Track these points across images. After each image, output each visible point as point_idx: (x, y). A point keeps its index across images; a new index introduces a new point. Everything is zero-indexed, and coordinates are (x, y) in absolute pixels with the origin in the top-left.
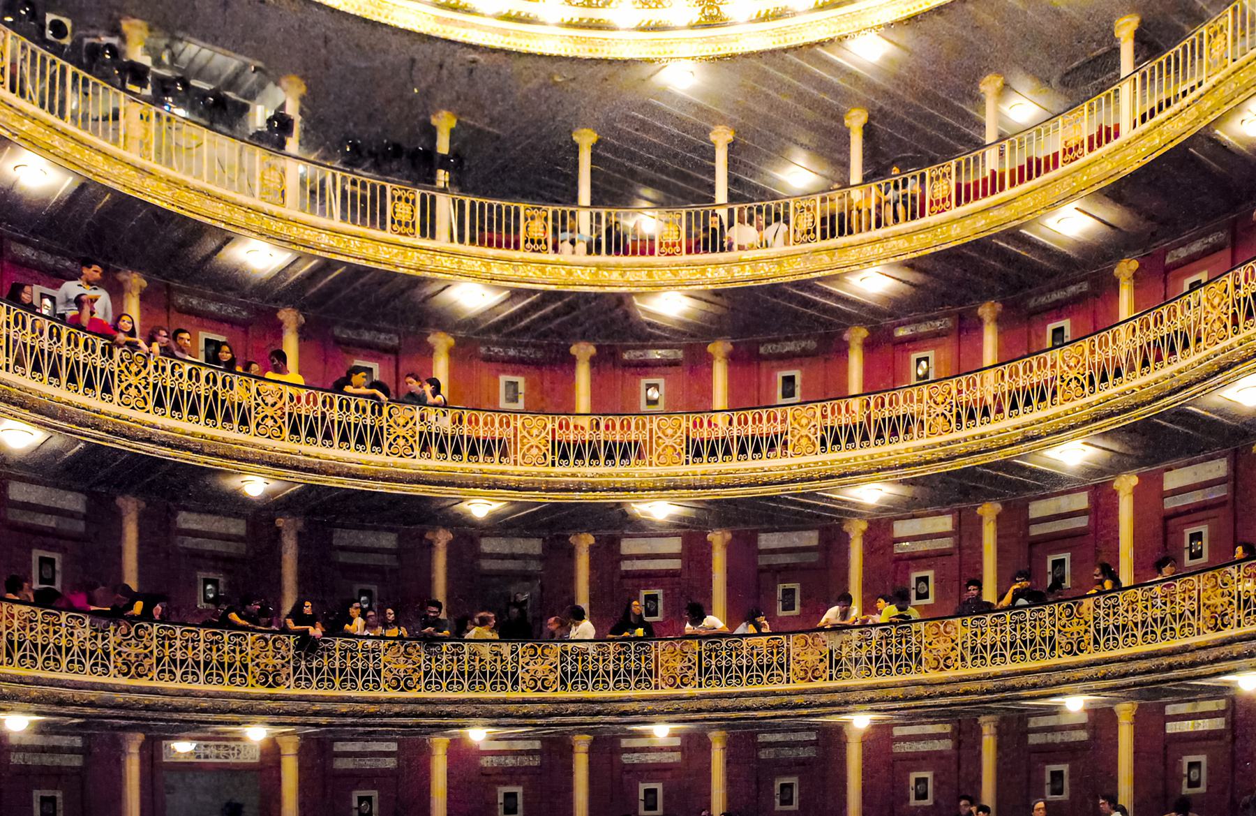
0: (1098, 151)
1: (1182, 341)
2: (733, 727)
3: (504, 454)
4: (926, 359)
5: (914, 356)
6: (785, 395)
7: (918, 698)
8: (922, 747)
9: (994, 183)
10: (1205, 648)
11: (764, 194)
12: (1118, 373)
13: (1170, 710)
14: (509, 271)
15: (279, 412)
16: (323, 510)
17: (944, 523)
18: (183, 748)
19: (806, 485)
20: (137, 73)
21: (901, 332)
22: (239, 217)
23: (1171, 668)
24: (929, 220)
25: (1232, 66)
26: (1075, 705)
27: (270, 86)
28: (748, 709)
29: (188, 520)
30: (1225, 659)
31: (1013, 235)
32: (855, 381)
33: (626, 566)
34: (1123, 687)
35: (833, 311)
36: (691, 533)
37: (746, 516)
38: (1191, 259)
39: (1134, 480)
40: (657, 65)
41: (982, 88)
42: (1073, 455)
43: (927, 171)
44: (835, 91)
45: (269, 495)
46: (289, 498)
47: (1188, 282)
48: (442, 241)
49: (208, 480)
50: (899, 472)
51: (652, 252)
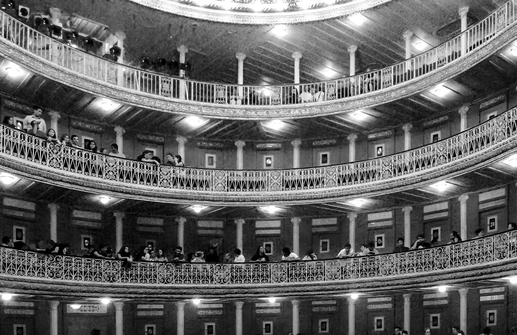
0: (452, 62)
1: (487, 140)
2: (302, 298)
3: (207, 186)
4: (381, 147)
5: (376, 146)
6: (323, 162)
7: (378, 287)
8: (380, 307)
9: (410, 75)
10: (496, 266)
11: (314, 80)
12: (460, 153)
13: (481, 291)
14: (209, 112)
15: (115, 169)
16: (133, 209)
17: (389, 215)
18: (75, 307)
19: (332, 199)
20: (57, 30)
21: (371, 136)
23: (482, 274)
24: (382, 90)
25: (507, 27)
26: (443, 289)
27: (111, 35)
29: (77, 214)
31: (417, 97)
33: (258, 232)
36: (285, 219)
37: (308, 212)
38: (490, 106)
39: (467, 197)
40: (270, 27)
41: (404, 36)
42: (442, 187)
44: (344, 38)
46: (119, 204)
48: (182, 99)
49: (86, 197)
50: (370, 194)
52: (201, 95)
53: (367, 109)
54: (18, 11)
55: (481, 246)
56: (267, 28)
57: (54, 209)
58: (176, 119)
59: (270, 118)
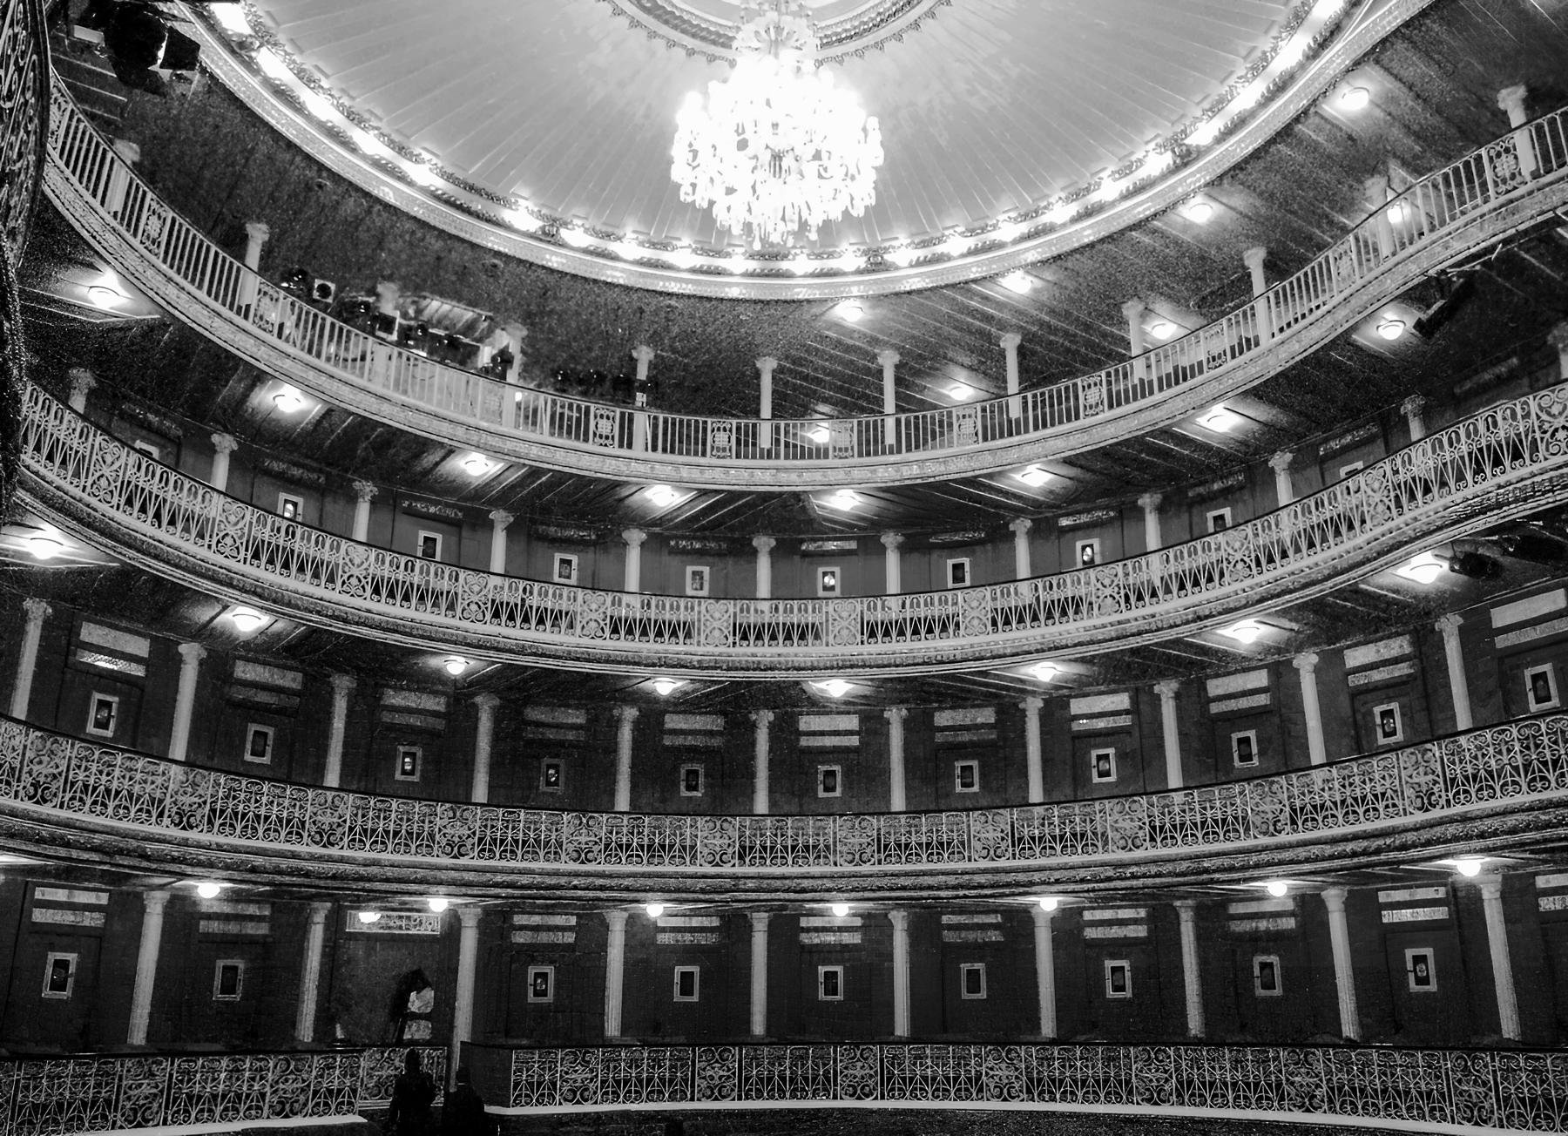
0: (1240, 360)
1: (1341, 525)
3: (688, 635)
4: (1091, 546)
8: (1116, 932)
9: (1145, 389)
12: (1284, 555)
14: (695, 474)
16: (520, 687)
17: (1122, 701)
18: (368, 918)
19: (978, 663)
20: (387, 323)
22: (460, 432)
23: (1378, 851)
24: (1083, 422)
25: (1360, 282)
26: (1278, 889)
27: (498, 331)
28: (930, 888)
30: (1438, 842)
31: (1166, 433)
32: (1023, 567)
34: (1330, 871)
35: (998, 505)
36: (869, 711)
37: (922, 693)
38: (1345, 450)
39: (1314, 659)
41: (1125, 312)
42: (1246, 633)
43: (1079, 381)
45: (468, 675)
46: (489, 677)
47: (1343, 471)
48: (638, 450)
51: (826, 457)
52: (669, 441)
53: (1057, 462)
54: (310, 290)
55: (1367, 776)
56: (816, 310)
57: (343, 684)
58: (625, 492)
59: (832, 487)
